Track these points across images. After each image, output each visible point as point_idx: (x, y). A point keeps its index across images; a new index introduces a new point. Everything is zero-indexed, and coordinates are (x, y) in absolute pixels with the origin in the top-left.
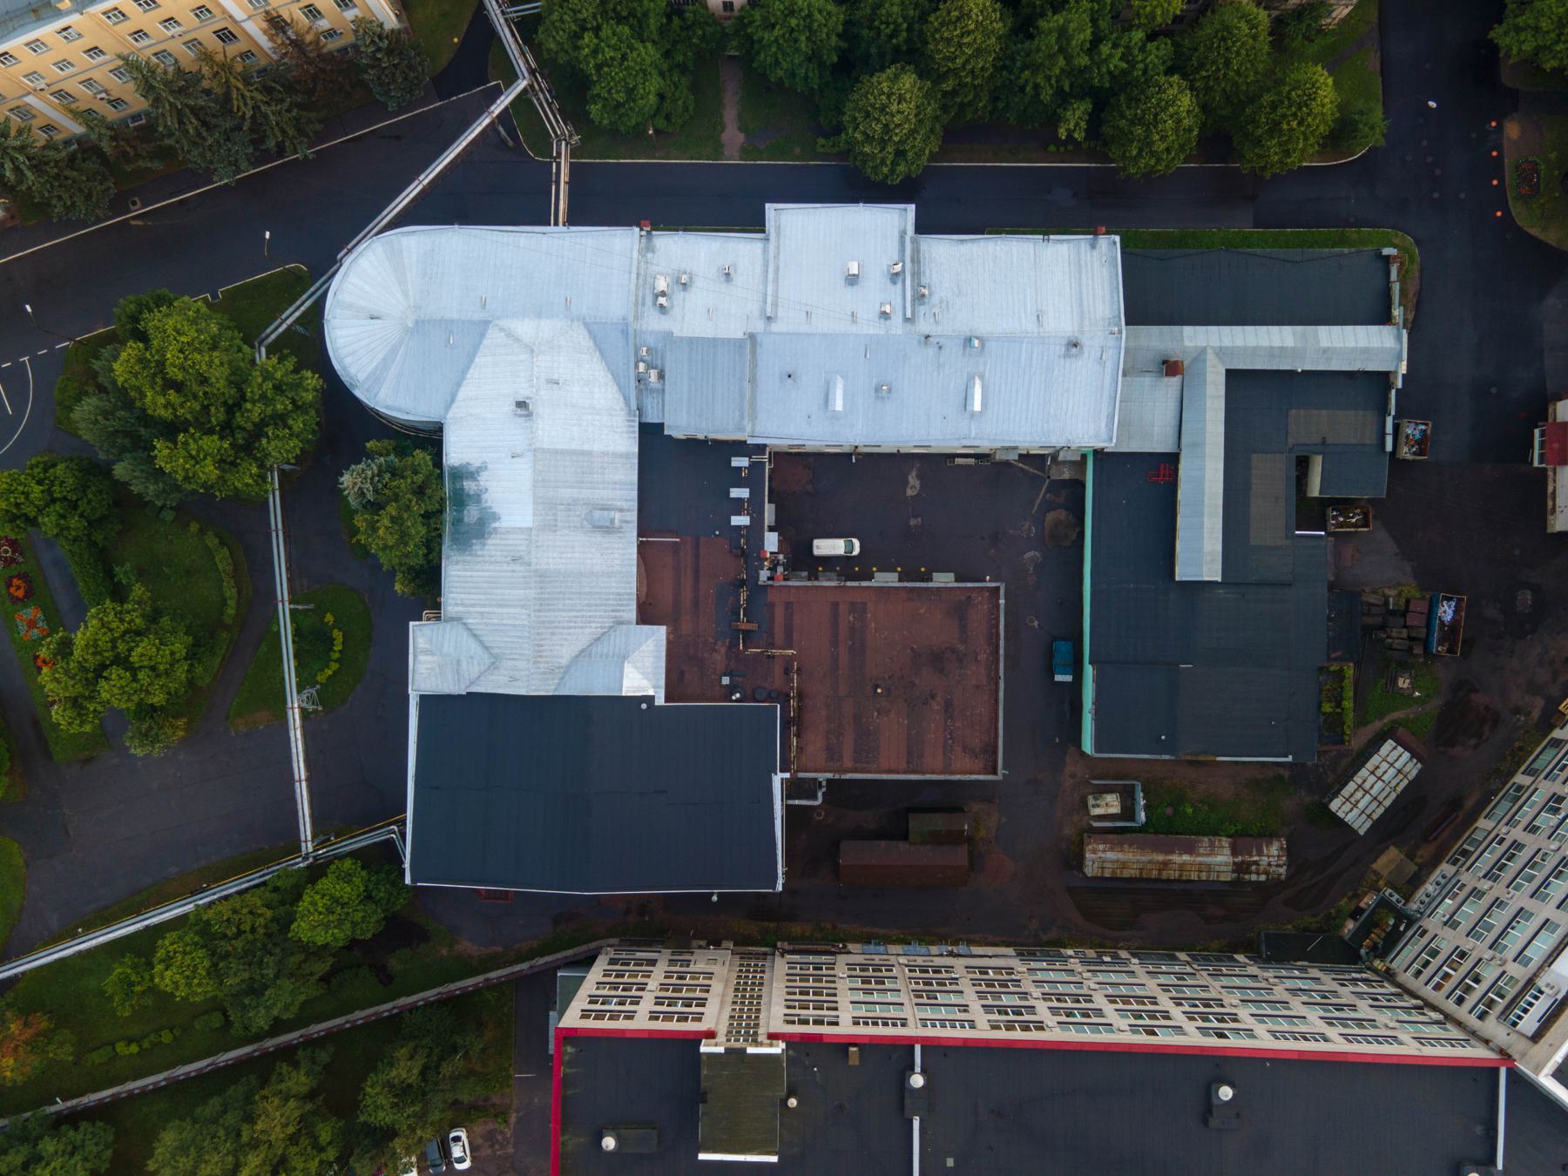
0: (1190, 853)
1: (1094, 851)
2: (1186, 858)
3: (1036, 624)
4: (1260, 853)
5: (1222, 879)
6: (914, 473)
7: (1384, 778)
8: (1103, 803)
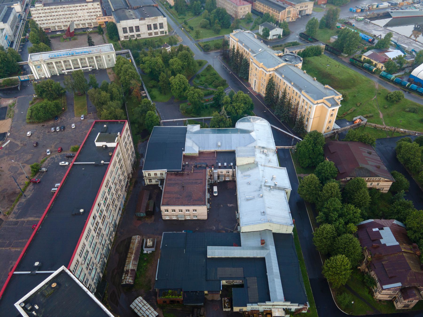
0: (133, 259)
1: (138, 237)
2: (133, 258)
3: (197, 229)
4: (130, 277)
5: (125, 268)
6: (233, 205)
7: (147, 311)
8: (150, 241)
